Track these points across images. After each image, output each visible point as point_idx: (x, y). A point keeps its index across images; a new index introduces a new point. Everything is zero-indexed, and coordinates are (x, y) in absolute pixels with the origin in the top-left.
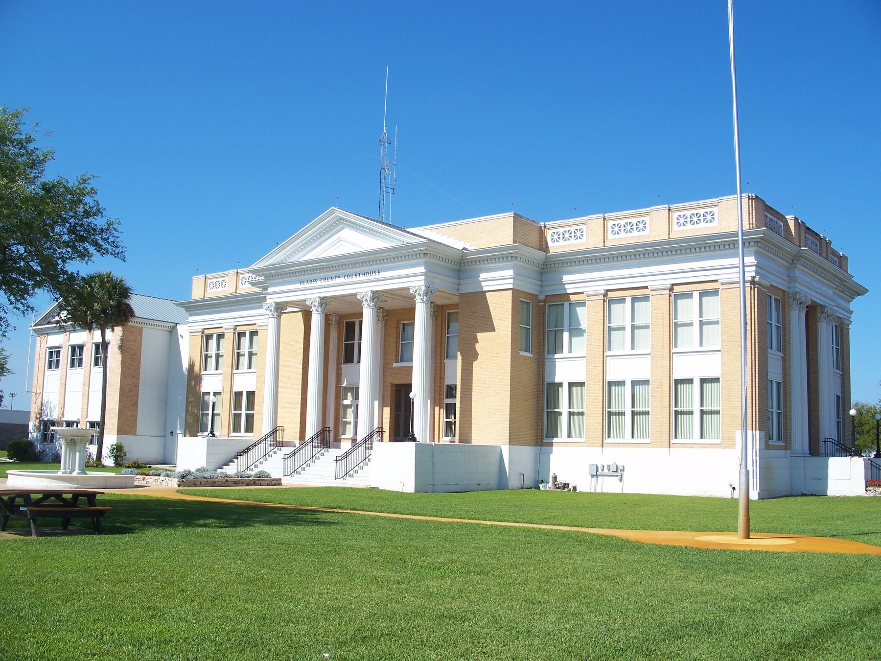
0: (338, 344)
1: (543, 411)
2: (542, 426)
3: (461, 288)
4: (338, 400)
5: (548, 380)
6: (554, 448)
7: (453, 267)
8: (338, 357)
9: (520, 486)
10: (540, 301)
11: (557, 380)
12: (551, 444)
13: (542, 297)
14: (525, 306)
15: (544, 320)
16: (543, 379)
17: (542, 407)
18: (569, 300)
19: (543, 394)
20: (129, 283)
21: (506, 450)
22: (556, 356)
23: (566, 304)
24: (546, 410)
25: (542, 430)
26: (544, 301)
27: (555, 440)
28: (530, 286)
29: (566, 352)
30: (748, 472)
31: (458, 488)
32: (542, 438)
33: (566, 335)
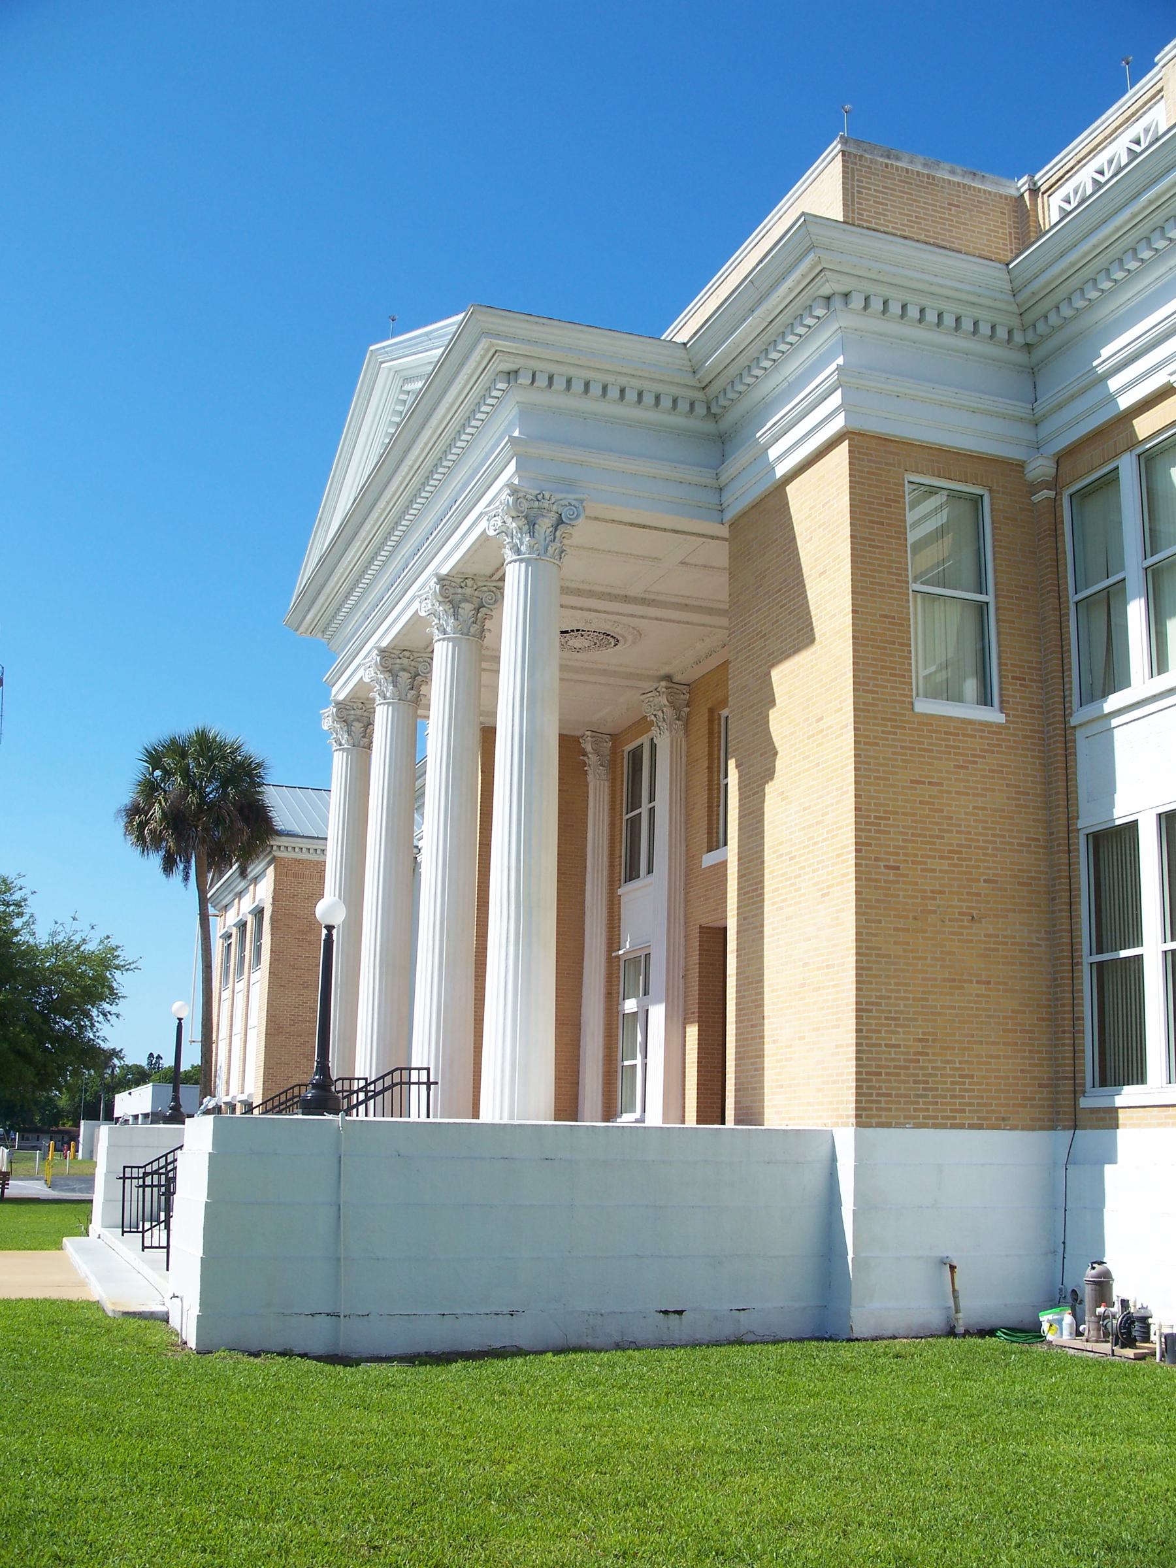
0: (612, 825)
1: (1074, 964)
2: (1076, 1033)
3: (727, 498)
4: (612, 1000)
5: (1088, 822)
6: (1120, 1132)
7: (677, 420)
8: (612, 866)
9: (936, 1320)
10: (1033, 488)
11: (1121, 813)
12: (1108, 1119)
13: (1040, 467)
14: (965, 507)
15: (1058, 562)
16: (1071, 816)
17: (1073, 946)
18: (1132, 442)
19: (1072, 891)
20: (254, 747)
21: (846, 1140)
22: (1112, 702)
23: (1127, 466)
24: (1088, 958)
25: (1077, 1053)
26: (1055, 483)
27: (1128, 1095)
28: (962, 417)
29: (1141, 680)
30: (895, 1338)
31: (439, 1336)
32: (1077, 1091)
33: (1136, 612)
